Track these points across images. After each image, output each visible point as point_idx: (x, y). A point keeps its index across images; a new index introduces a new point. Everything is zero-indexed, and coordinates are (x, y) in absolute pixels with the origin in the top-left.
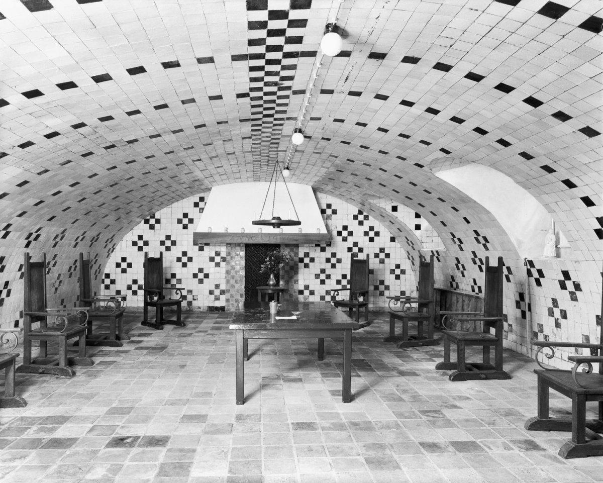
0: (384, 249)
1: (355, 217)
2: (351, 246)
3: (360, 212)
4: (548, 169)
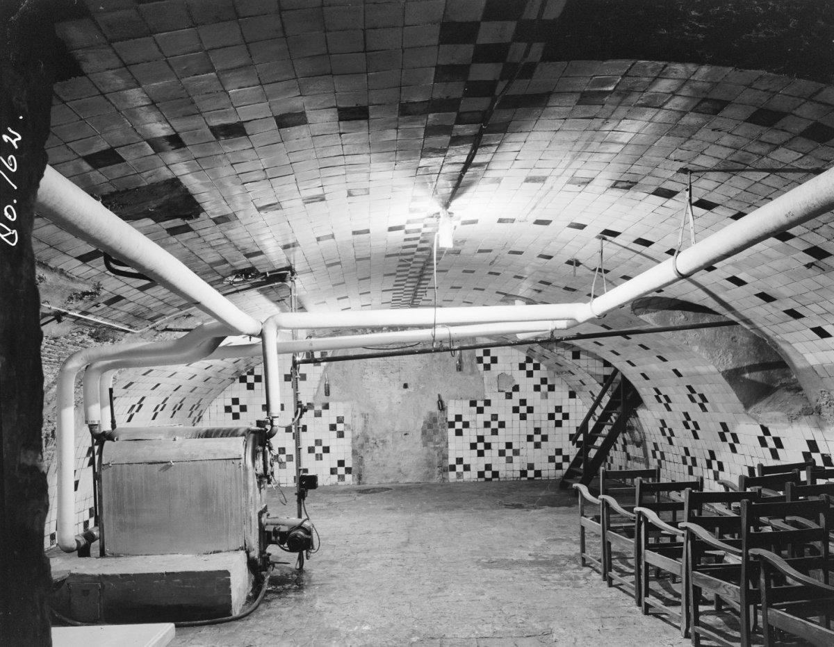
0: (561, 407)
1: (522, 367)
2: (517, 404)
3: (529, 360)
4: (794, 314)
